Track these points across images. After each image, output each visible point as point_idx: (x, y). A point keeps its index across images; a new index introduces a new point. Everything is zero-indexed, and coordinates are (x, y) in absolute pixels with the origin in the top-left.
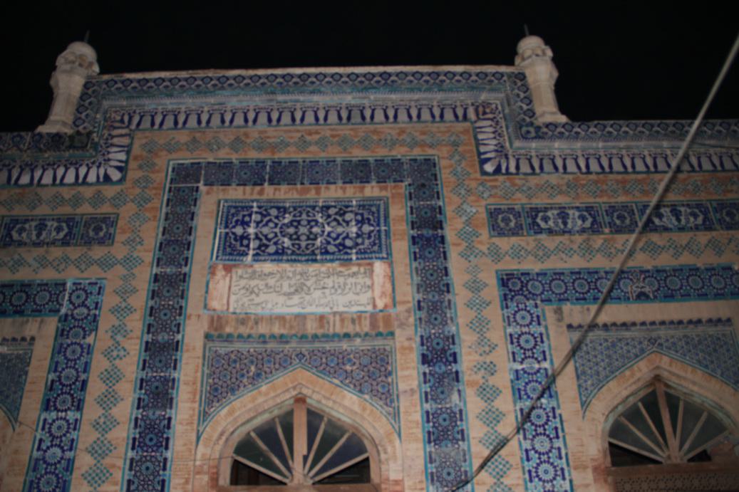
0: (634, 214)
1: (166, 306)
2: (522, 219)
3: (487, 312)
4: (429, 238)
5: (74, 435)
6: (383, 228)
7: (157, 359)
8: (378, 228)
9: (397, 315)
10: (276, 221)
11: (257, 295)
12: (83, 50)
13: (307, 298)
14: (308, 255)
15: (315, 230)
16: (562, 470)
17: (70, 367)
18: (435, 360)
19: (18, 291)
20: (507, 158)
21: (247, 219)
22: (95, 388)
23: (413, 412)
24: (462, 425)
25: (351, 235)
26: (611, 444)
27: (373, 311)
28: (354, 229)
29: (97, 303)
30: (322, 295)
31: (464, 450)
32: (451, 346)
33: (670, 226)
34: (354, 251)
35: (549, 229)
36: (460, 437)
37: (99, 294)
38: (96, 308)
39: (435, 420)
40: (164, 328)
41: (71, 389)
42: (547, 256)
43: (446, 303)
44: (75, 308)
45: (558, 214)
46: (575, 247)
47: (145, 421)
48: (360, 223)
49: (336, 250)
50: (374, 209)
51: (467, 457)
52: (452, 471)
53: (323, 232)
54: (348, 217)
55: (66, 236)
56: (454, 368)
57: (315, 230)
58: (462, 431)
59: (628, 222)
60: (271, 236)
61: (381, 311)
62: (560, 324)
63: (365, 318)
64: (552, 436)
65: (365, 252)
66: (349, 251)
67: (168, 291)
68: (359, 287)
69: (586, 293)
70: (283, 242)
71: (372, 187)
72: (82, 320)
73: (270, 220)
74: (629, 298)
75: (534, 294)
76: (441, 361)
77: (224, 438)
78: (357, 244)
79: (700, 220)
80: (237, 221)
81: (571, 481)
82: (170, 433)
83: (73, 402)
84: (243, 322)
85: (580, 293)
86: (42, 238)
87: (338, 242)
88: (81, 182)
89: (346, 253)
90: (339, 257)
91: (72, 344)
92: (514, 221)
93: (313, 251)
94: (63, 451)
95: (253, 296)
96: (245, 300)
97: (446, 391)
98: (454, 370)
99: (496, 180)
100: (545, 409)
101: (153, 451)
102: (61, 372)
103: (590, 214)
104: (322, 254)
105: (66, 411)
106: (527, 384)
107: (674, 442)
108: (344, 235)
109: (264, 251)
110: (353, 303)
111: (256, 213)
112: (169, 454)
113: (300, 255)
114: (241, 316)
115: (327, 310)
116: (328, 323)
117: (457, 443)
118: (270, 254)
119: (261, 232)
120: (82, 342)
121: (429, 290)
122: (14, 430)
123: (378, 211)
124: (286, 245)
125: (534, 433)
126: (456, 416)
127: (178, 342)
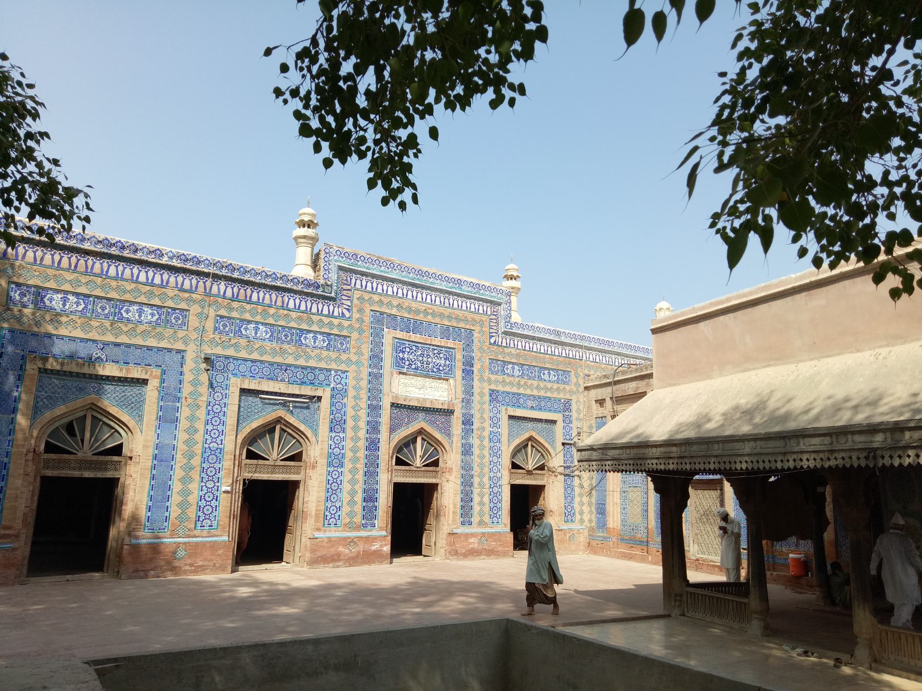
5: (344, 443)
12: (881, 87)
22: (350, 423)
40: (375, 398)
48: (446, 359)
54: (442, 355)
59: (180, 322)
82: (380, 445)
88: (297, 309)
107: (530, 461)
112: (379, 453)
126: (471, 446)
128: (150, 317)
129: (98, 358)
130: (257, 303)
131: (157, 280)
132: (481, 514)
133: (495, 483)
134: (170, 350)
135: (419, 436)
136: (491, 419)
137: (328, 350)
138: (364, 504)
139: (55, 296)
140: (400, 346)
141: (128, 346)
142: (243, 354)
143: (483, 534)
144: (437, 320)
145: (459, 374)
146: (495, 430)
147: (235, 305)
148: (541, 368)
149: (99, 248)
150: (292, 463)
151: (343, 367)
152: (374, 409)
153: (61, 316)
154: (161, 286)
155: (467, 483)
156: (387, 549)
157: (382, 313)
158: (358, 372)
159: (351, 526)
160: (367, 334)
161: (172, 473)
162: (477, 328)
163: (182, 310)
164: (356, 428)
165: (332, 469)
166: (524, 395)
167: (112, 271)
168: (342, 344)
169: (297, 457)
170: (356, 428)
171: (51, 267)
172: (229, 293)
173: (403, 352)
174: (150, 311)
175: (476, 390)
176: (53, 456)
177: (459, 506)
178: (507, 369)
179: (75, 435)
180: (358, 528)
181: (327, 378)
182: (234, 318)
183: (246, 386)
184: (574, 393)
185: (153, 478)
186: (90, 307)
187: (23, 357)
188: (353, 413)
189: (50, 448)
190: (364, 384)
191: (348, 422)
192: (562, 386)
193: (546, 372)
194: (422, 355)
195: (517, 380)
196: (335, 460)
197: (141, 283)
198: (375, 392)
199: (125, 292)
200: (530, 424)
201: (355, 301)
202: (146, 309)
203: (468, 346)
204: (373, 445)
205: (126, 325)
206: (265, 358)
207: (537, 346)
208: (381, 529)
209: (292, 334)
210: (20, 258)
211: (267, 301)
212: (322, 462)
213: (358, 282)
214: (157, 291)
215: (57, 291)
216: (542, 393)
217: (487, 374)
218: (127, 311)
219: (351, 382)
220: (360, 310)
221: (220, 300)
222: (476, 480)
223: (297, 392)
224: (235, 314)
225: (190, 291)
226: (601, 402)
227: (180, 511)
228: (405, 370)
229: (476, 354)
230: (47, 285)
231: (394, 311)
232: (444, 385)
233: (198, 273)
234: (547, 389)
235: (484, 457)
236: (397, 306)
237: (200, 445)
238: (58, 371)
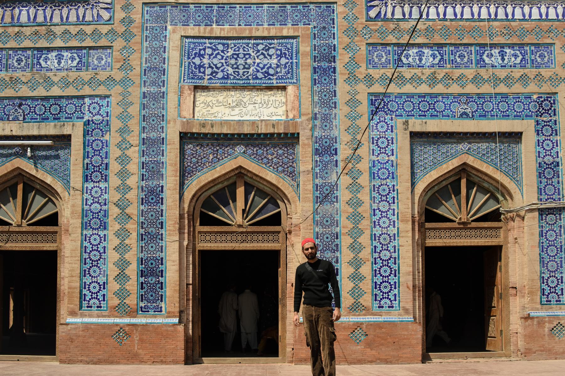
0: (471, 54)
1: (153, 115)
2: (391, 56)
4: (324, 66)
6: (295, 61)
7: (151, 150)
8: (291, 61)
9: (302, 122)
10: (222, 54)
11: (212, 108)
13: (244, 110)
14: (245, 79)
15: (249, 61)
16: (394, 222)
17: (97, 155)
18: (323, 153)
19: (53, 104)
20: (386, 6)
21: (202, 52)
23: (306, 183)
24: (337, 193)
25: (273, 66)
26: (426, 209)
27: (286, 119)
28: (275, 61)
29: (107, 112)
30: (253, 108)
31: (337, 208)
32: (334, 144)
33: (496, 64)
34: (275, 77)
35: (409, 64)
36: (335, 200)
37: (108, 106)
38: (107, 116)
39: (321, 190)
40: (153, 129)
41: (99, 169)
42: (67, 85)
43: (333, 115)
44: (94, 116)
46: (424, 78)
47: (148, 188)
48: (280, 56)
49: (263, 76)
50: (289, 46)
51: (339, 212)
52: (329, 219)
53: (254, 63)
54: (272, 51)
55: (78, 64)
56: (335, 158)
57: (249, 61)
58: (337, 196)
59: (466, 60)
60: (219, 65)
61: (291, 120)
62: (406, 132)
63: (281, 124)
64: (390, 202)
65: (282, 78)
66: (271, 77)
67: (154, 104)
68: (277, 103)
69: (426, 112)
70: (228, 70)
71: (288, 29)
72: (100, 124)
73: (218, 54)
74: (455, 116)
75: (391, 111)
76: (327, 153)
77: (195, 199)
78: (277, 73)
80: (196, 54)
81: (398, 228)
82: (163, 195)
83: (102, 177)
84: (204, 125)
85: (422, 111)
86: (62, 65)
87: (264, 70)
88: (81, 21)
89: (270, 79)
90: (265, 81)
91: (95, 140)
93: (247, 77)
94: (101, 206)
95: (209, 108)
96: (204, 111)
97: (329, 172)
98: (335, 159)
99: (377, 25)
100: (388, 186)
101: (154, 206)
102: (91, 158)
103: (440, 53)
104: (253, 79)
105: (98, 182)
106: (379, 170)
108: (269, 65)
109: (214, 77)
110: (273, 114)
111: (209, 47)
113: (239, 79)
114: (202, 122)
115: (257, 118)
116: (258, 127)
117: (333, 204)
118: (219, 79)
119: (212, 63)
120: (102, 139)
121: (323, 106)
122: (69, 194)
123: (292, 47)
124: (229, 72)
125: (380, 200)
127: (163, 139)
131: (518, 15)
132: (356, 292)
138: (142, 280)
140: (193, 48)
145: (305, 75)
151: (101, 90)
152: (153, 145)
158: (125, 95)
159: (121, 309)
164: (123, 174)
165: (90, 232)
170: (123, 174)
173: (201, 56)
180: (132, 313)
181: (79, 109)
188: (118, 153)
191: (111, 167)
194: (236, 56)
198: (153, 118)
200: (463, 146)
204: (153, 196)
208: (170, 315)
209: (27, 58)
212: (77, 222)
216: (486, 89)
219: (115, 110)
223: (35, 132)
228: (205, 83)
229: (340, 40)
232: (279, 96)
235: (360, 203)
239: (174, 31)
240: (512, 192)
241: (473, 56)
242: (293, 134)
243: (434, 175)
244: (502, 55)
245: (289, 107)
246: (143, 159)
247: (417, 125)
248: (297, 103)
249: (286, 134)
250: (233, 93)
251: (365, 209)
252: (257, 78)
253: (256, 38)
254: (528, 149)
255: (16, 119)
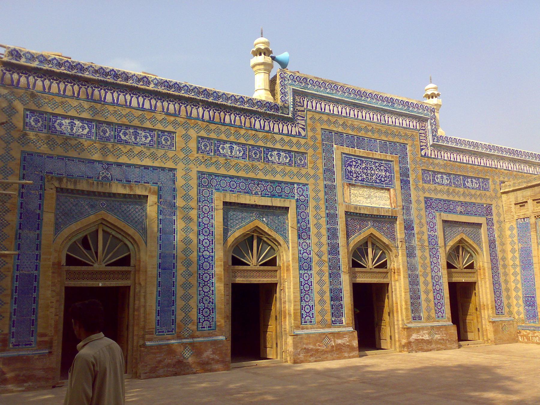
3: (421, 213)
15: (372, 172)
22: (313, 231)
40: (332, 208)
42: (285, 175)
45: (69, 123)
57: (372, 172)
59: (169, 143)
78: (385, 180)
79: (288, 161)
88: (262, 129)
92: (41, 122)
126: (413, 248)
128: (144, 139)
129: (105, 177)
130: (230, 125)
132: (428, 310)
133: (436, 283)
134: (163, 169)
135: (368, 242)
136: (428, 223)
137: (290, 165)
139: (63, 121)
140: (348, 161)
141: (129, 166)
142: (223, 171)
143: (432, 327)
144: (376, 136)
145: (397, 184)
146: (432, 233)
147: (212, 127)
148: (464, 176)
149: (97, 77)
150: (269, 268)
151: (303, 181)
152: (332, 217)
153: (71, 139)
154: (151, 110)
155: (413, 281)
156: (355, 343)
157: (331, 132)
158: (316, 185)
159: (323, 323)
160: (320, 150)
161: (174, 279)
162: (409, 142)
163: (170, 132)
166: (454, 202)
167: (109, 98)
168: (301, 160)
169: (272, 262)
171: (58, 95)
172: (206, 117)
173: (351, 166)
174: (143, 134)
175: (413, 198)
176: (73, 268)
177: (409, 303)
178: (437, 178)
179: (90, 249)
182: (212, 139)
183: (228, 200)
184: (494, 198)
185: (159, 284)
186: (94, 131)
187: (42, 178)
188: (315, 222)
189: (70, 261)
190: (322, 195)
192: (483, 192)
193: (469, 180)
195: (446, 187)
196: (304, 264)
197: (134, 108)
198: (331, 202)
199: (121, 116)
201: (309, 121)
202: (140, 132)
203: (404, 157)
204: (334, 250)
205: (125, 147)
206: (241, 174)
207: (459, 158)
208: (348, 325)
210: (31, 87)
211: (238, 123)
213: (309, 104)
214: (148, 115)
215: (65, 117)
216: (467, 200)
217: (421, 183)
218: (125, 134)
219: (311, 193)
220: (313, 129)
221: (200, 122)
222: (421, 279)
224: (213, 135)
225: (174, 115)
226: (522, 204)
227: (184, 315)
228: (353, 182)
230: (56, 111)
231: (340, 129)
232: (386, 194)
233: (180, 99)
234: (471, 195)
236: (342, 125)
237: (195, 254)
238: (72, 190)
239: (338, 149)
240: (141, 248)
241: (262, 154)
242: (395, 217)
243: (237, 234)
244: (136, 134)
245: (392, 202)
246: (328, 226)
247: (232, 198)
248: (395, 198)
249: (392, 216)
250: (366, 189)
251: (428, 260)
252: (376, 183)
253: (375, 159)
254: (483, 231)
255: (256, 194)
